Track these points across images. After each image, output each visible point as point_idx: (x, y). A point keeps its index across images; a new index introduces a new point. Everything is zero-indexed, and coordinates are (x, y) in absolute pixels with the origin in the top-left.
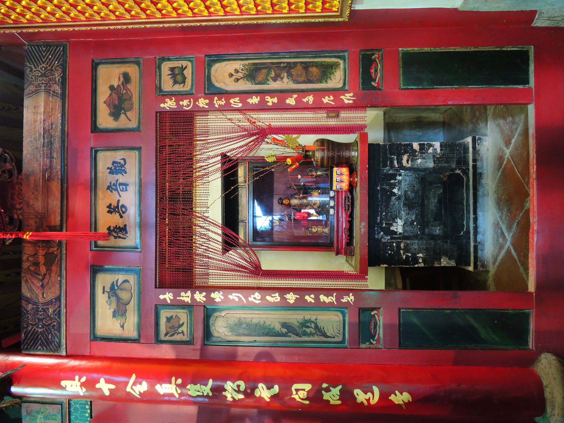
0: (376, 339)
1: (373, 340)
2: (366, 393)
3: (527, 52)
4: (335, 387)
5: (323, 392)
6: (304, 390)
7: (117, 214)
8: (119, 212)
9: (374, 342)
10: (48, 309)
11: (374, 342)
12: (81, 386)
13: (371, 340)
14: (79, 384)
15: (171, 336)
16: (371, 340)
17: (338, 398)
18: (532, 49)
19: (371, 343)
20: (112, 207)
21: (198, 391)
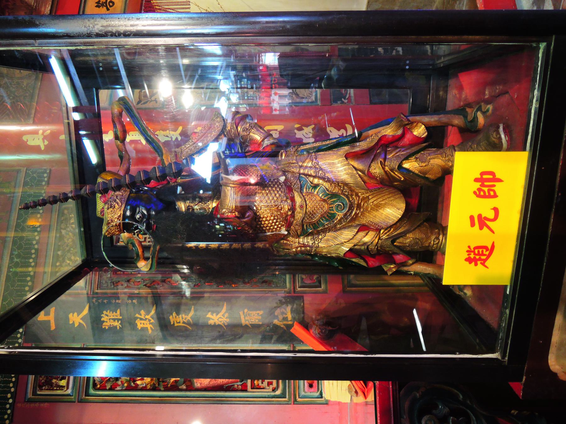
0: (347, 97)
1: (345, 99)
2: (339, 130)
3: (285, 398)
4: (307, 126)
5: (296, 131)
6: (276, 130)
7: (105, 8)
8: (106, 6)
9: (346, 101)
10: (23, 82)
11: (346, 101)
12: (43, 139)
13: (343, 99)
14: (42, 137)
15: (144, 103)
16: (343, 99)
17: (311, 135)
18: (286, 399)
19: (343, 102)
20: (101, 2)
21: (167, 136)
